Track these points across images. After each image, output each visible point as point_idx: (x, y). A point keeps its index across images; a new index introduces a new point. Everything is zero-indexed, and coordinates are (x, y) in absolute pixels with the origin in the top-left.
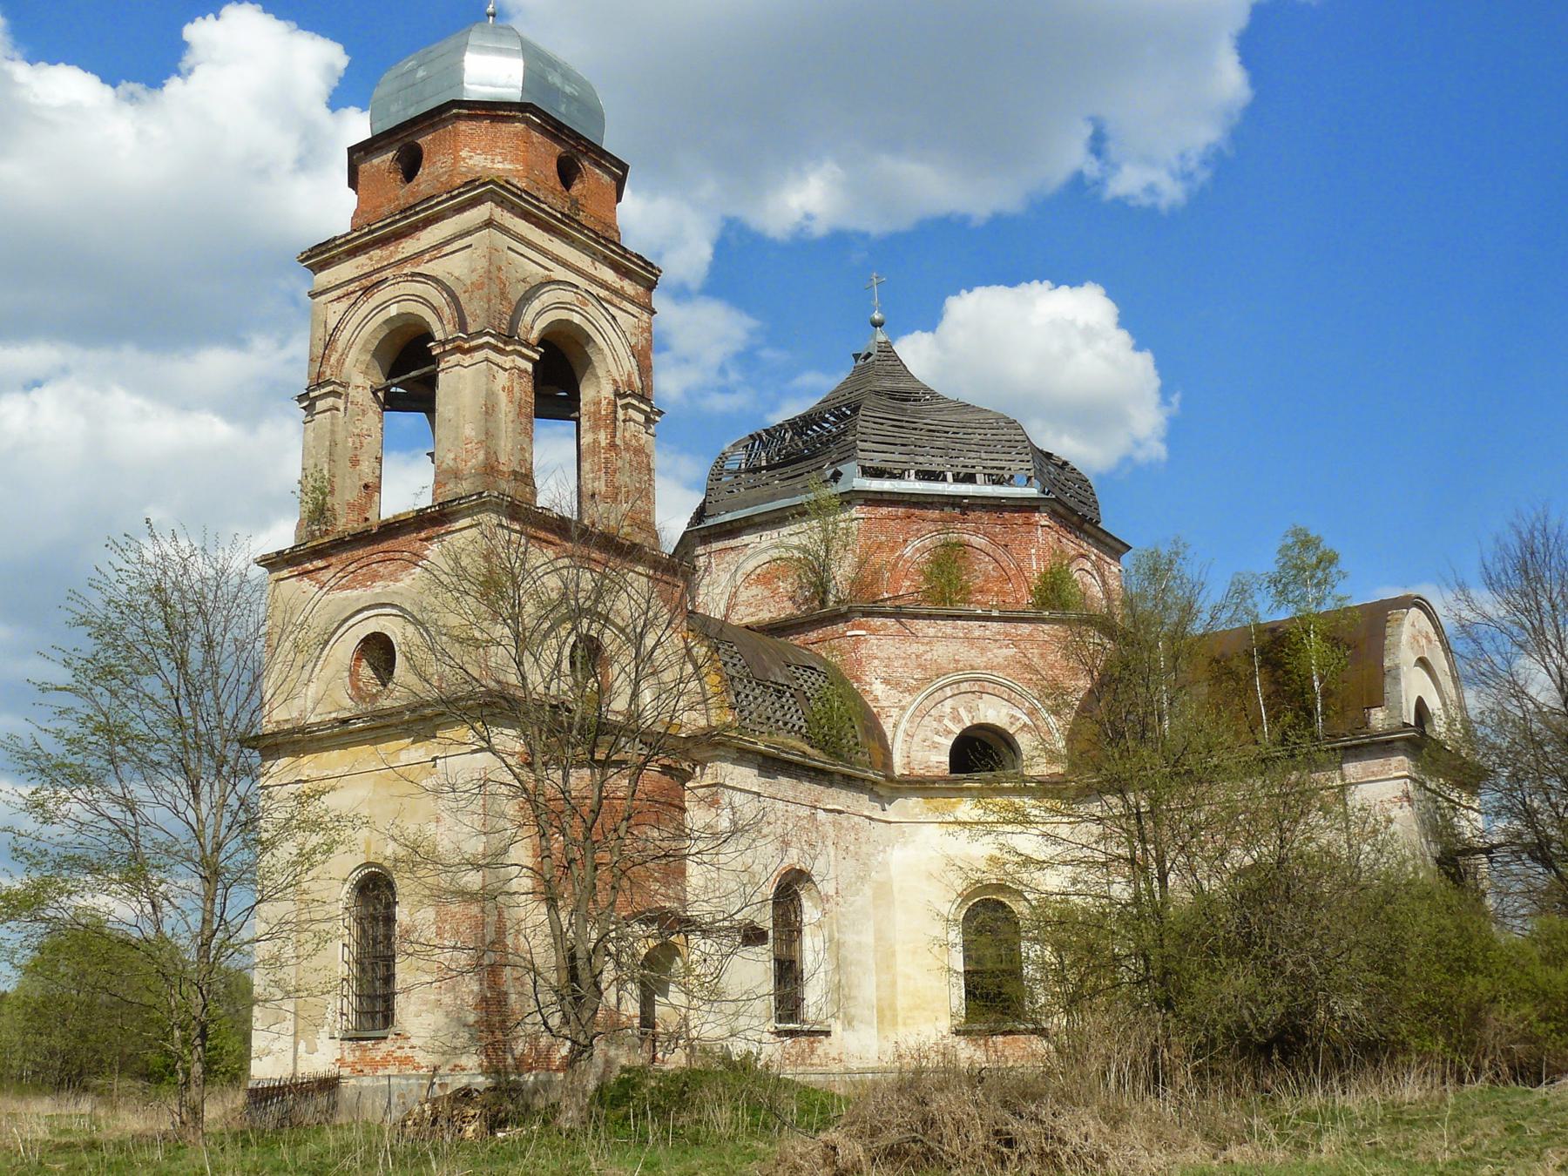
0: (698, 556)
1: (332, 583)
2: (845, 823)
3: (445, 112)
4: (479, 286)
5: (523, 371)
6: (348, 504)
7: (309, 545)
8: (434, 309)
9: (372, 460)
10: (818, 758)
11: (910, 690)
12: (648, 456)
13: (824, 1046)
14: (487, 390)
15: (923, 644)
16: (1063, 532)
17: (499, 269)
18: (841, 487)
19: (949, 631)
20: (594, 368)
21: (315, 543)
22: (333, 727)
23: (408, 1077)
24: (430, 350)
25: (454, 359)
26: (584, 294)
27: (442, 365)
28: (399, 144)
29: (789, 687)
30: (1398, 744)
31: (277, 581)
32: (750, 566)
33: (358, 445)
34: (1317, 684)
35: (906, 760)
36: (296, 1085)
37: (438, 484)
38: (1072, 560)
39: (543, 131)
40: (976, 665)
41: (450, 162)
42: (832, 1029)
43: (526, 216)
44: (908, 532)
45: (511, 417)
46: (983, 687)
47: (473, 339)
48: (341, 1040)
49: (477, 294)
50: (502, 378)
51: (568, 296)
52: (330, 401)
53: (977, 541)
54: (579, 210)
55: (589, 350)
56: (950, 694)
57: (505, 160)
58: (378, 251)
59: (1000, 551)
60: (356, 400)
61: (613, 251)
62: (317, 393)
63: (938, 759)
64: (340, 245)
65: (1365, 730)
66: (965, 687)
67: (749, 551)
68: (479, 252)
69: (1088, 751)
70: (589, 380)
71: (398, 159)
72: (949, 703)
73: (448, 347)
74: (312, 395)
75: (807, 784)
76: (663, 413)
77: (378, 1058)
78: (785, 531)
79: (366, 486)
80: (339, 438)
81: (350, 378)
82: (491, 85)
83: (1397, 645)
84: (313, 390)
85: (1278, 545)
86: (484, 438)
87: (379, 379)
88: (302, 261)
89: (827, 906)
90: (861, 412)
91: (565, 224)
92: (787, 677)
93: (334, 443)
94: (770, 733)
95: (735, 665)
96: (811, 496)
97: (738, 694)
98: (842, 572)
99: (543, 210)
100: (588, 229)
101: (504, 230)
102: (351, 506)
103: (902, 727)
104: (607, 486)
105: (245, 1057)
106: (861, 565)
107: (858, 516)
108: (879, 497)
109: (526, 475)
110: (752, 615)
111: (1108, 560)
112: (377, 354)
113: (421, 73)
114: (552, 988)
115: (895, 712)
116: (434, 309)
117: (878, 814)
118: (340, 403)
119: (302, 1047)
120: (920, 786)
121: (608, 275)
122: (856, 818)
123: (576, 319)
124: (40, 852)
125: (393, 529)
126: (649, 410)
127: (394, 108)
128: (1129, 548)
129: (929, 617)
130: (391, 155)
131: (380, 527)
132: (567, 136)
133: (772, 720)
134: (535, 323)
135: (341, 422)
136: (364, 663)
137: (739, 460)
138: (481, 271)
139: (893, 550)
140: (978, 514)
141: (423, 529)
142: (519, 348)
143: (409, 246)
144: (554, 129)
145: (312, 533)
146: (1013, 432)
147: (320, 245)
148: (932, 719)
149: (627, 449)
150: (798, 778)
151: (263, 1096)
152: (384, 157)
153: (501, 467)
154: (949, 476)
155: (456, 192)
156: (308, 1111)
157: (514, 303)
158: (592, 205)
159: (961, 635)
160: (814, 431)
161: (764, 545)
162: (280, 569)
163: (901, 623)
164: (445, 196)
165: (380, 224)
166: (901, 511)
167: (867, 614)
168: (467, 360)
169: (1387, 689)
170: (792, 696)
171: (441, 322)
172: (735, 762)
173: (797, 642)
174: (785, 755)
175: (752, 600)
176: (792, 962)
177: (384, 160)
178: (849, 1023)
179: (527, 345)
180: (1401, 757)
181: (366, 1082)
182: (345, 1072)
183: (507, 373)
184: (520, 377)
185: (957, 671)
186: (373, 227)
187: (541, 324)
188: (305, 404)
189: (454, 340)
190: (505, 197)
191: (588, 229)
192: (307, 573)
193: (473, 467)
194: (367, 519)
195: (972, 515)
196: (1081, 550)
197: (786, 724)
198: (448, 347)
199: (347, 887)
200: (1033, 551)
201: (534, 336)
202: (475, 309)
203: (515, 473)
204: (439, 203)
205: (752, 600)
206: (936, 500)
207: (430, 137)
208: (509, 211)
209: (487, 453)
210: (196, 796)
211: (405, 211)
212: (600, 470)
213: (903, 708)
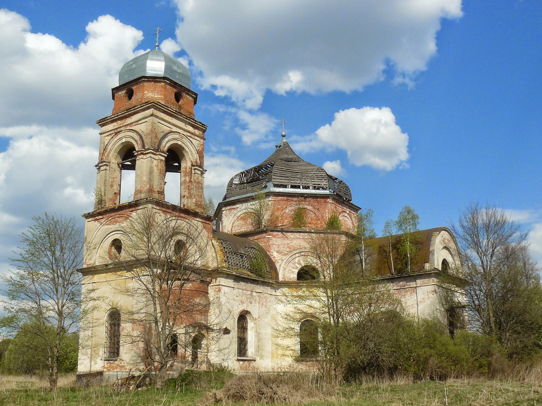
0: (223, 211)
1: (104, 223)
2: (262, 296)
3: (140, 79)
4: (149, 134)
5: (162, 160)
6: (110, 199)
7: (97, 211)
8: (136, 141)
9: (117, 185)
10: (253, 276)
11: (285, 255)
12: (202, 184)
13: (253, 364)
14: (150, 166)
15: (289, 240)
16: (337, 204)
17: (155, 129)
18: (266, 191)
19: (298, 236)
20: (185, 157)
21: (99, 211)
22: (103, 267)
23: (123, 372)
24: (134, 153)
25: (142, 156)
26: (182, 135)
27: (137, 158)
28: (127, 88)
29: (245, 254)
30: (433, 274)
31: (88, 222)
32: (239, 214)
33: (113, 181)
34: (409, 255)
35: (283, 276)
36: (91, 374)
37: (135, 194)
38: (340, 213)
39: (170, 85)
40: (306, 247)
41: (141, 95)
42: (256, 359)
43: (164, 112)
44: (287, 205)
45: (158, 174)
46: (308, 254)
47: (146, 151)
48: (104, 360)
49: (148, 136)
50: (155, 162)
51: (177, 136)
52: (105, 167)
53: (309, 207)
54: (181, 109)
55: (184, 152)
56: (298, 256)
57: (158, 94)
58: (120, 122)
59: (316, 211)
60: (112, 167)
61: (192, 121)
62: (101, 165)
63: (294, 276)
64: (109, 119)
65: (423, 270)
66: (303, 253)
67: (238, 210)
68: (149, 123)
69: (469, 241)
70: (184, 161)
71: (126, 93)
72: (297, 259)
73: (139, 153)
74: (99, 165)
75: (250, 284)
76: (207, 171)
77: (114, 366)
78: (249, 204)
79: (115, 193)
80: (107, 178)
81: (111, 160)
82: (155, 71)
83: (434, 243)
84: (100, 164)
85: (401, 210)
86: (149, 181)
87: (120, 160)
88: (97, 123)
89: (256, 322)
90: (274, 166)
91: (176, 114)
92: (245, 251)
93: (106, 180)
94: (238, 269)
95: (228, 248)
96: (257, 193)
97: (227, 257)
98: (266, 217)
99: (169, 110)
100: (184, 115)
101: (157, 117)
102: (110, 199)
103: (282, 266)
104: (188, 194)
105: (76, 365)
106: (271, 215)
107: (272, 199)
108: (278, 194)
109: (162, 192)
110: (239, 230)
111: (353, 212)
112: (119, 153)
113: (134, 66)
114: (156, 347)
115: (280, 261)
116: (136, 141)
117: (274, 293)
118: (108, 168)
119: (93, 363)
120: (287, 284)
121: (190, 129)
122: (266, 295)
123: (179, 143)
124: (11, 308)
125: (122, 208)
126: (202, 170)
127: (126, 77)
128: (361, 209)
129: (292, 232)
130: (124, 92)
131: (118, 207)
132: (177, 86)
133: (239, 265)
134: (166, 145)
135: (108, 173)
136: (113, 248)
137: (236, 181)
138: (149, 130)
139: (282, 210)
140: (310, 199)
141: (130, 208)
142: (160, 153)
143: (129, 121)
144: (174, 84)
145: (99, 208)
146: (322, 173)
147: (103, 119)
148: (292, 264)
149: (195, 182)
150: (247, 282)
151: (80, 377)
152: (122, 92)
153: (154, 190)
154: (301, 187)
155: (142, 105)
156: (94, 380)
157: (160, 139)
158: (185, 107)
159: (302, 238)
160: (261, 171)
161: (243, 208)
162: (89, 218)
163: (283, 234)
164: (139, 106)
165: (120, 113)
166: (285, 198)
167: (272, 231)
168: (145, 157)
169: (430, 257)
170: (246, 257)
171: (138, 145)
172: (226, 278)
173: (251, 239)
174: (242, 276)
175: (239, 225)
176: (245, 339)
177: (122, 93)
178: (262, 357)
179: (163, 152)
180: (433, 279)
181: (111, 373)
182: (105, 370)
183: (157, 161)
184: (161, 162)
185: (300, 249)
186: (118, 114)
187: (168, 145)
188: (97, 168)
189: (141, 151)
190: (157, 107)
191: (184, 115)
192: (97, 219)
193: (146, 190)
194: (115, 204)
195: (308, 199)
196: (344, 210)
197: (243, 266)
198: (139, 153)
199: (107, 314)
200: (327, 211)
201: (166, 149)
202: (147, 141)
203: (158, 191)
204: (137, 108)
205: (239, 225)
206: (296, 194)
207: (136, 87)
208: (158, 111)
209: (150, 186)
210: (57, 291)
211: (128, 110)
212: (186, 189)
213: (283, 260)
